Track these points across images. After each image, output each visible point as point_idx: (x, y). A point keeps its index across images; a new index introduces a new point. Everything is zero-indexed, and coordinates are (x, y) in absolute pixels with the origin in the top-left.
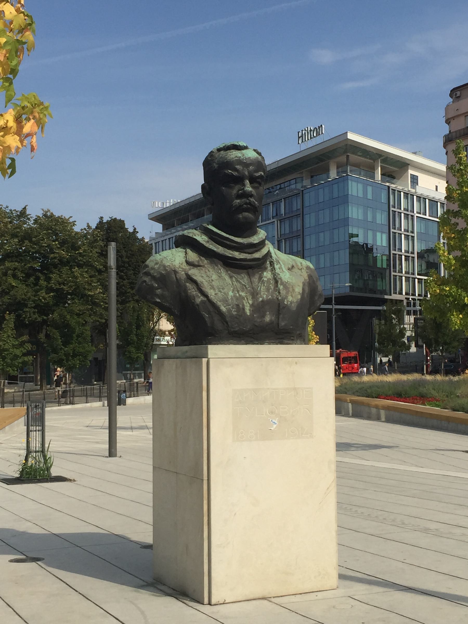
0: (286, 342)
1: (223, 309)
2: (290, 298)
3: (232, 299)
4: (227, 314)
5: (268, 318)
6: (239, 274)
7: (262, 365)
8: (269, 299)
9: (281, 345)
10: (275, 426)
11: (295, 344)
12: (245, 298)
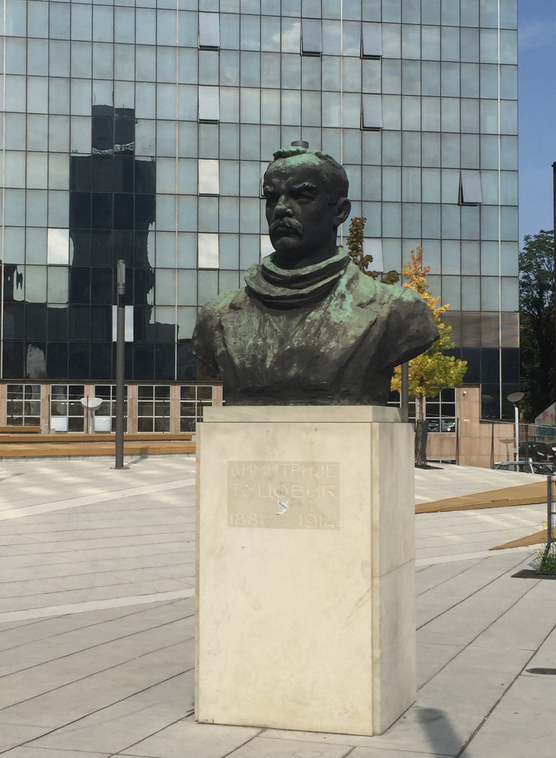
0: (320, 401)
1: (237, 361)
2: (333, 344)
3: (250, 348)
4: (239, 367)
5: (293, 372)
6: (278, 315)
7: (268, 431)
8: (302, 346)
9: (312, 407)
10: (284, 510)
11: (336, 405)
12: (272, 347)
